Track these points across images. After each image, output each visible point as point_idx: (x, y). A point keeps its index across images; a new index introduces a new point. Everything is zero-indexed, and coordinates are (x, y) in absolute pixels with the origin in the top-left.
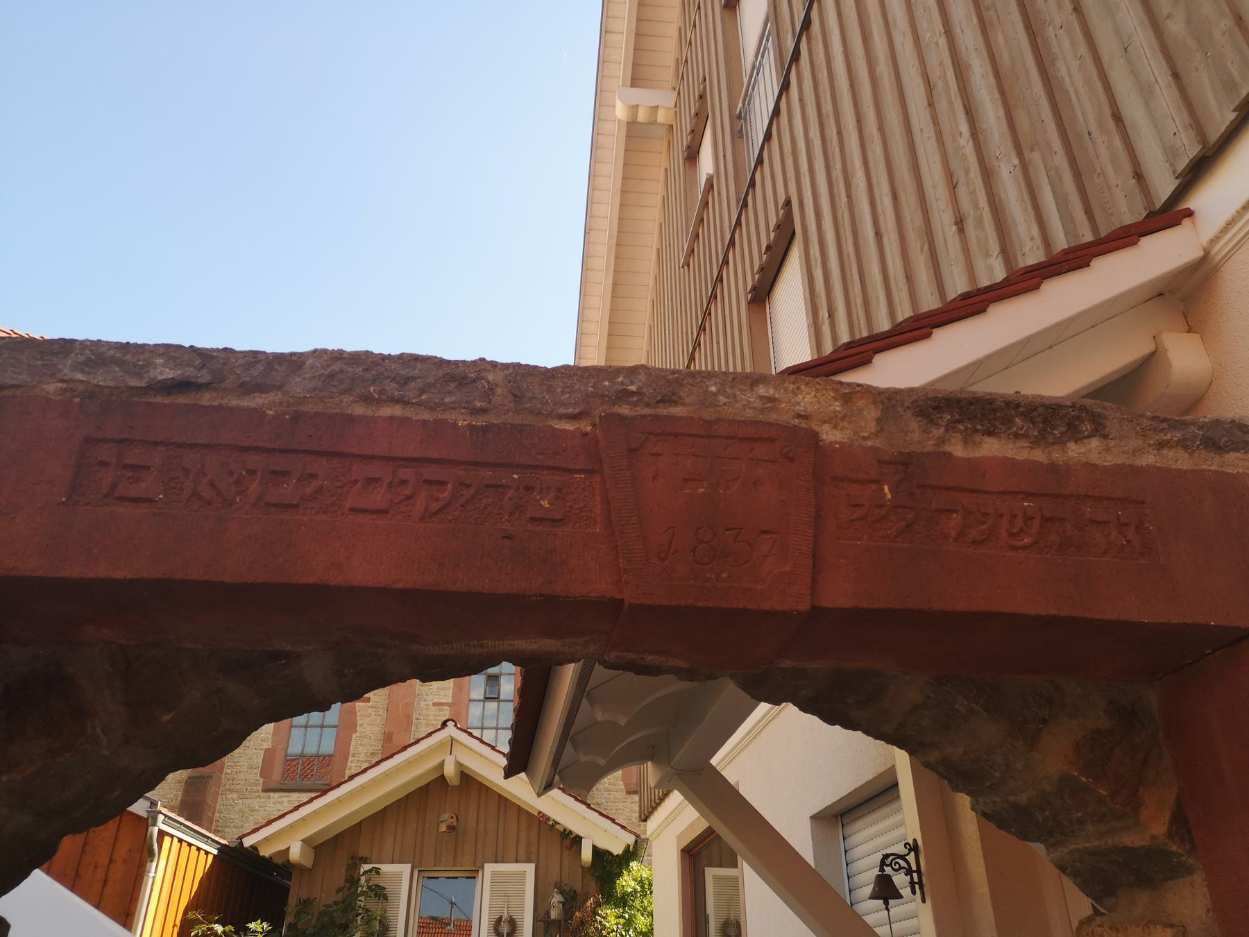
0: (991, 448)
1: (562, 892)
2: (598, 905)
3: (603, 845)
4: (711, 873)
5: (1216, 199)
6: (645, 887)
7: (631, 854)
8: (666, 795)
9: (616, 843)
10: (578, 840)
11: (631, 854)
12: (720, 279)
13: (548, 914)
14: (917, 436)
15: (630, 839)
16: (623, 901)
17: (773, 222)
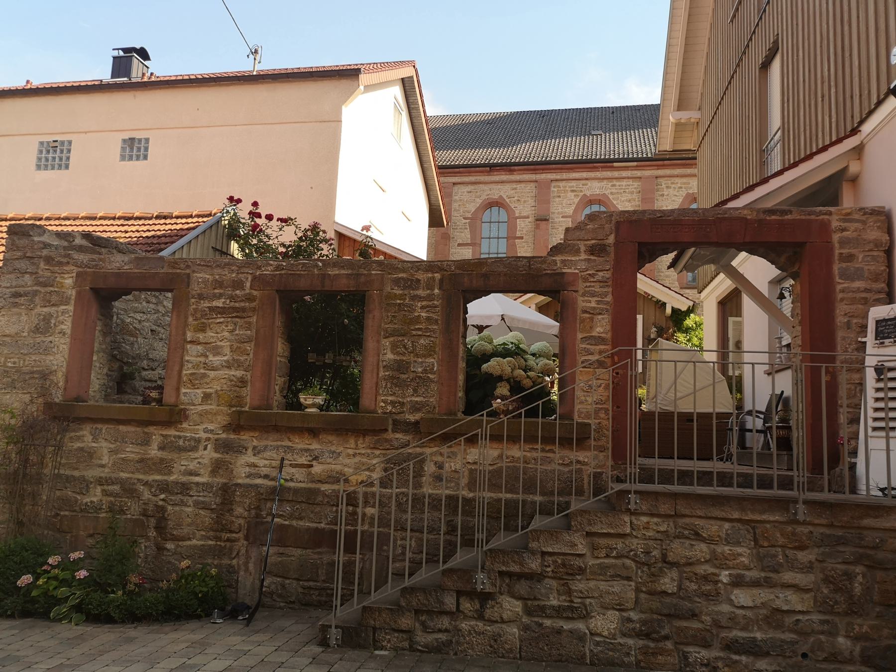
0: (773, 217)
1: (655, 327)
2: (675, 332)
3: (676, 306)
4: (731, 320)
5: (867, 128)
6: (699, 325)
7: (690, 311)
8: (718, 274)
9: (683, 305)
10: (664, 304)
11: (690, 311)
12: (748, 46)
13: (649, 336)
14: (762, 216)
15: (691, 304)
16: (687, 330)
17: (772, 41)
